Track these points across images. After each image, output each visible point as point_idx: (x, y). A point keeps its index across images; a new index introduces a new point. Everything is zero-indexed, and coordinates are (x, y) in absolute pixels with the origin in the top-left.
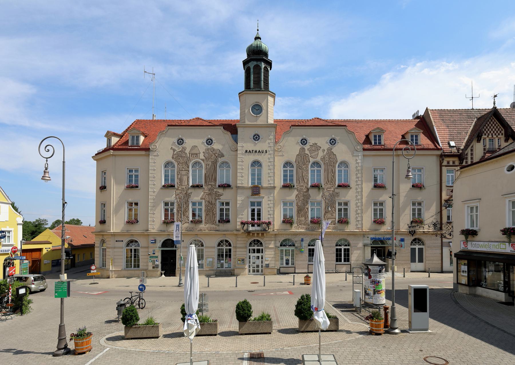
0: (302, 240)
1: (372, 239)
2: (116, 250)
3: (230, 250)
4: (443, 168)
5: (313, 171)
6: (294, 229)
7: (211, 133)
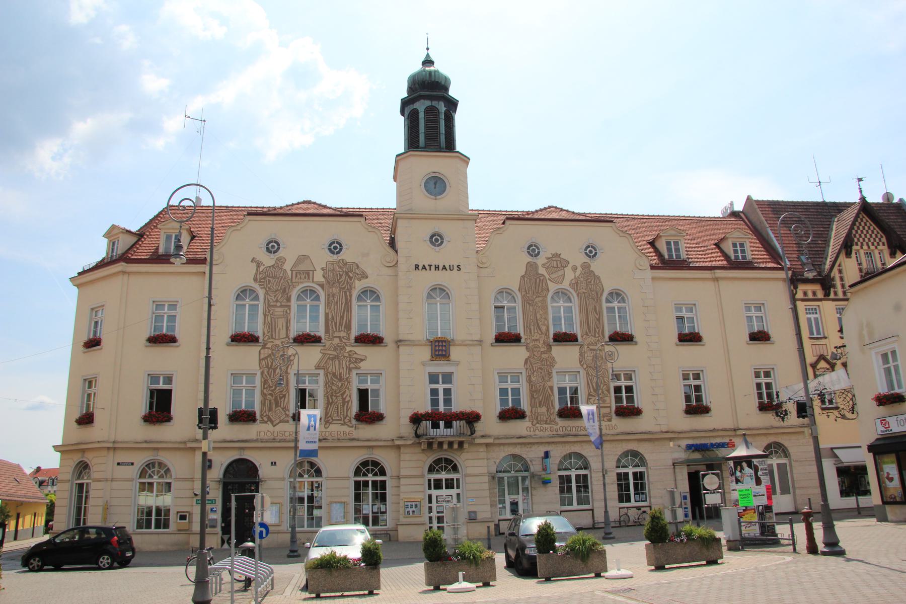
0: (547, 455)
2: (115, 485)
4: (799, 303)
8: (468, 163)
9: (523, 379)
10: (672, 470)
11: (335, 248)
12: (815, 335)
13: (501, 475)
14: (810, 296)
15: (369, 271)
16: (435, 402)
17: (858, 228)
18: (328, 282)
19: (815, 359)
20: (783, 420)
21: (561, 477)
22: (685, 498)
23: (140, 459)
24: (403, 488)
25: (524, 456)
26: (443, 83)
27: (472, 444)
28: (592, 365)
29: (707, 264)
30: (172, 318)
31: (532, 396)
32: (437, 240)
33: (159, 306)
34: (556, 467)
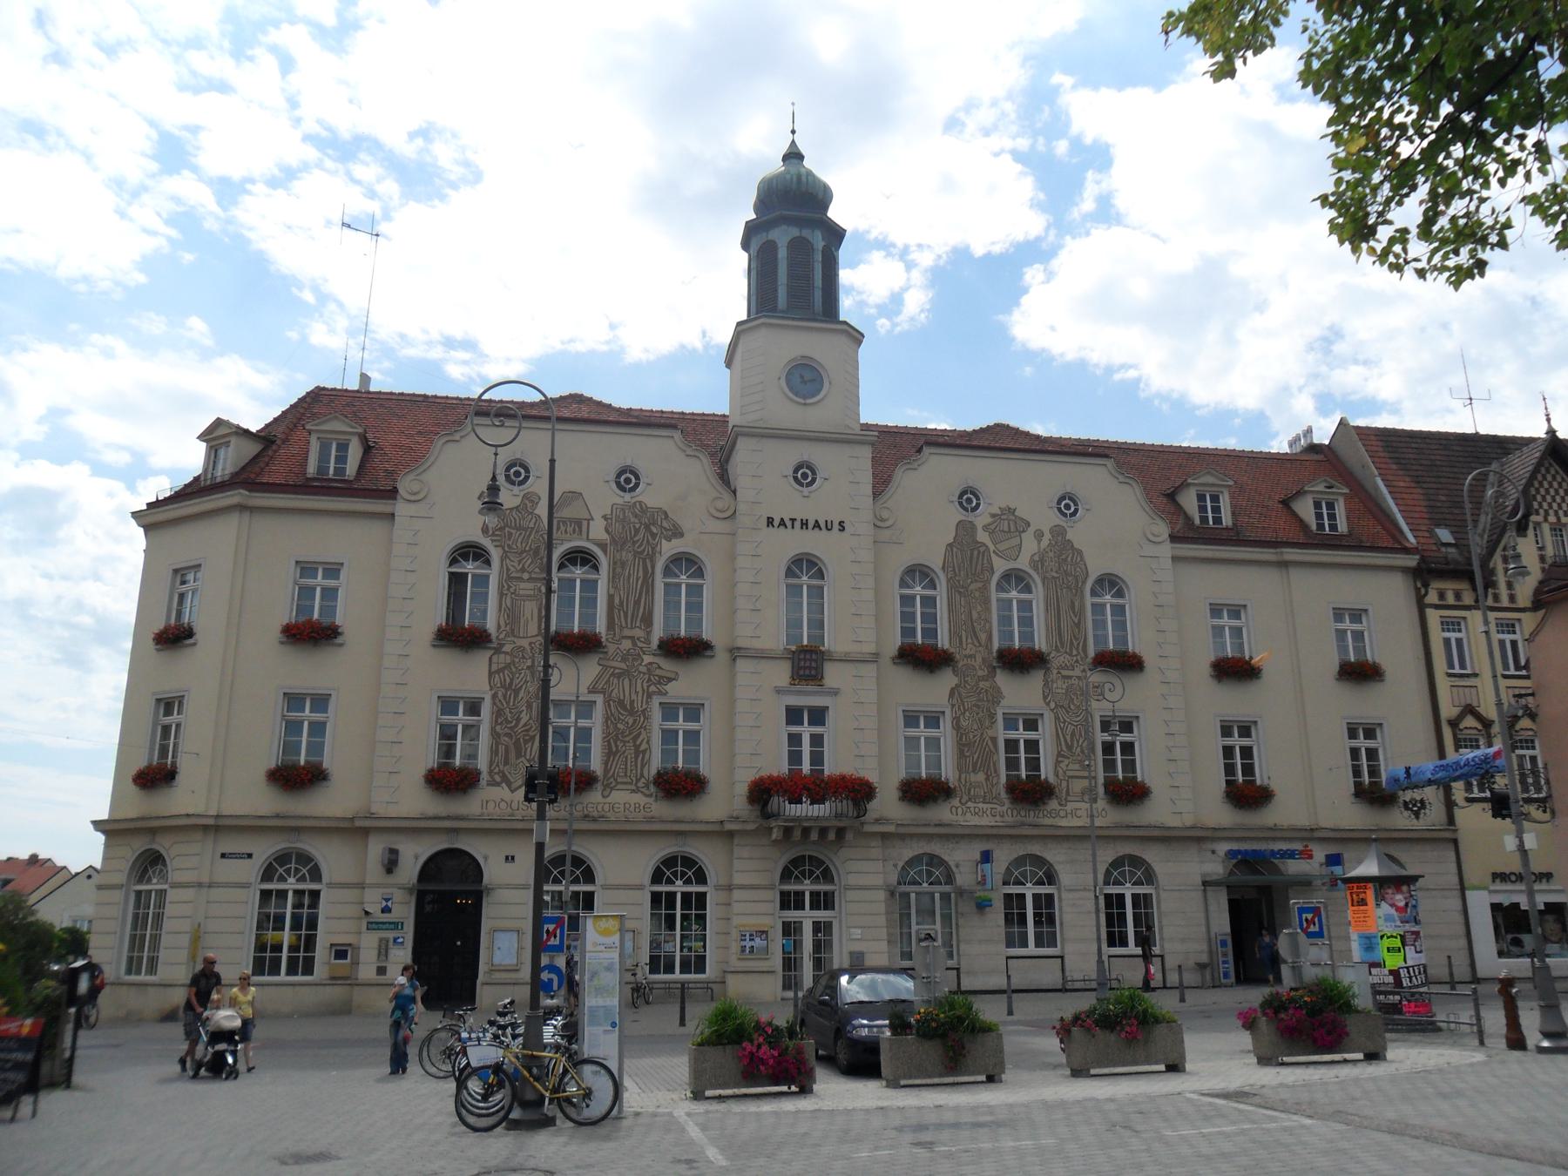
0: (986, 857)
1: (1231, 854)
2: (216, 893)
3: (315, 895)
4: (1430, 612)
5: (673, 590)
6: (472, 805)
7: (1089, 479)
8: (859, 342)
9: (946, 725)
10: (1200, 893)
11: (628, 481)
12: (1457, 670)
13: (903, 888)
14: (1451, 600)
15: (685, 525)
16: (795, 757)
17: (1541, 484)
18: (613, 540)
19: (1455, 712)
20: (1417, 818)
21: (1008, 897)
22: (1224, 944)
23: (265, 849)
24: (737, 908)
25: (946, 858)
26: (820, 196)
27: (860, 834)
28: (1066, 704)
29: (1270, 536)
30: (330, 594)
31: (961, 754)
32: (805, 476)
33: (307, 569)
34: (999, 879)
